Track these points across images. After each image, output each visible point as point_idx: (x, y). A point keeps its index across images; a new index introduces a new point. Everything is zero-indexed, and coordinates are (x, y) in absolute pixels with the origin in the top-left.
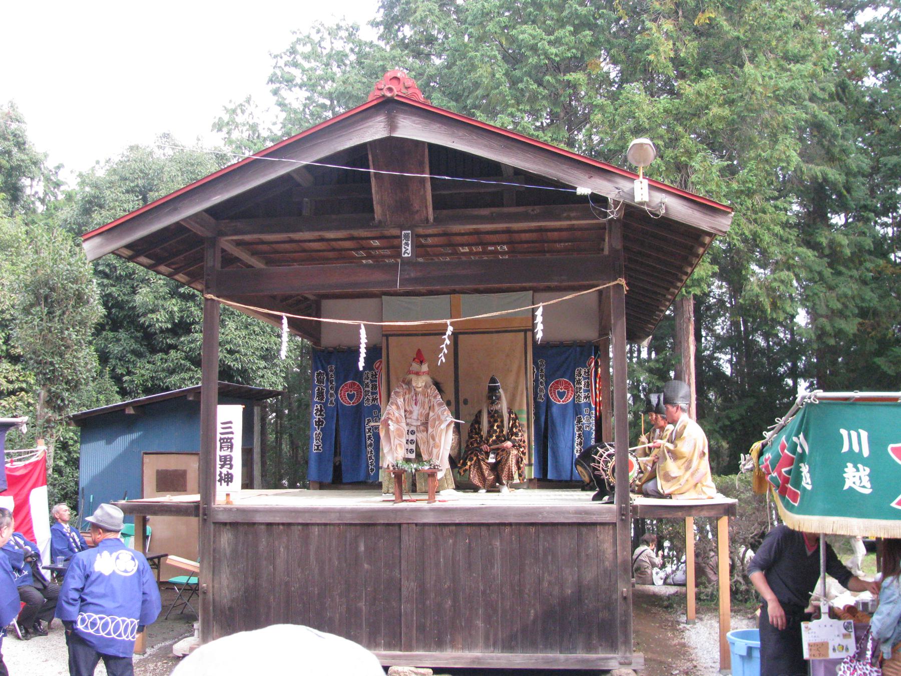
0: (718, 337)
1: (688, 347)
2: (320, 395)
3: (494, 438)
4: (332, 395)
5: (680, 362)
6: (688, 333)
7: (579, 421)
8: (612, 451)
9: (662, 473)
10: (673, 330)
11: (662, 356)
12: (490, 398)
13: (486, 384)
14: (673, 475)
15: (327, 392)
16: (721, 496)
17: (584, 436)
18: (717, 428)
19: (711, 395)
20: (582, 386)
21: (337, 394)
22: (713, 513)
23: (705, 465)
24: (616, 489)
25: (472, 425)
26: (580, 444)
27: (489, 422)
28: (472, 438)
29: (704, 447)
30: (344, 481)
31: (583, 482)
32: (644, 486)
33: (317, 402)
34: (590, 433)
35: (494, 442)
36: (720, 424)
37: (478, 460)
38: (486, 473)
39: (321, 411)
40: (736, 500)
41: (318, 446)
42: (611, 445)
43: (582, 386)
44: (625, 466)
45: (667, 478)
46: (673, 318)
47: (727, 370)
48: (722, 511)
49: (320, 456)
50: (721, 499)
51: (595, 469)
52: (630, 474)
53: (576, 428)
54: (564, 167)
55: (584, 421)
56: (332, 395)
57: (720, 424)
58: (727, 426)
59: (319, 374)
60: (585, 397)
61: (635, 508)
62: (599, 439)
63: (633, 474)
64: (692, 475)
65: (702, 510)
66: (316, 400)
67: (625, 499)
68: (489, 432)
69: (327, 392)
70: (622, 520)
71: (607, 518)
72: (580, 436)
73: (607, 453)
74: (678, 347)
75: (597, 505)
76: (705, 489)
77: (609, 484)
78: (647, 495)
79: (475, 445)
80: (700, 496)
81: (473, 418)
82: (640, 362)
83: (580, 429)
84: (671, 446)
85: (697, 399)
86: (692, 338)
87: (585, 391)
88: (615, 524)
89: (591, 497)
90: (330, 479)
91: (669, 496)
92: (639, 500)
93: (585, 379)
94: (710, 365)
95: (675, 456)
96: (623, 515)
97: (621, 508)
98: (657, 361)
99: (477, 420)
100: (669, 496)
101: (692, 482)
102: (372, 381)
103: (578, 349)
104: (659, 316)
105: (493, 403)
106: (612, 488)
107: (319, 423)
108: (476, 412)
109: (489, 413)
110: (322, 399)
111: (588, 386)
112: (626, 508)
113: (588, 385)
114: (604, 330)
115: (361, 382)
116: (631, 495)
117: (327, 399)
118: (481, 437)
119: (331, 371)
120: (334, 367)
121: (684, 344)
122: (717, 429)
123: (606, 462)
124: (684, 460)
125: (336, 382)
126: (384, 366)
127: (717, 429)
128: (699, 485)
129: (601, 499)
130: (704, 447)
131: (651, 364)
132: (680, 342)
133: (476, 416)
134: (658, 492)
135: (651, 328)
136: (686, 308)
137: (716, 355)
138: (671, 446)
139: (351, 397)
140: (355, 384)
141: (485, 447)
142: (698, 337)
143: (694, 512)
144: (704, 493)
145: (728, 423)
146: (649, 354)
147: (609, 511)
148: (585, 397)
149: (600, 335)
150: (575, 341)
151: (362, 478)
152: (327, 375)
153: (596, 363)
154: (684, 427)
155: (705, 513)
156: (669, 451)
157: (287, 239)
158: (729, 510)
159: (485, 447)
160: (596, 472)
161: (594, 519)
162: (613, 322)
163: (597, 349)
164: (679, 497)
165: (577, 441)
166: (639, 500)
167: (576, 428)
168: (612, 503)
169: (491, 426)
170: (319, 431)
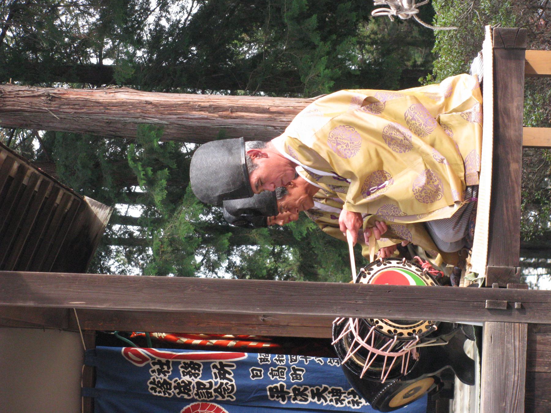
0: (103, 29)
1: (122, 104)
5: (159, 128)
6: (86, 103)
7: (281, 393)
8: (352, 325)
9: (418, 207)
10: (78, 137)
11: (139, 171)
14: (423, 180)
16: (476, 64)
17: (317, 385)
18: (324, 47)
19: (249, 51)
20: (194, 381)
22: (516, 87)
23: (398, 101)
24: (447, 319)
26: (336, 393)
29: (354, 101)
31: (431, 393)
32: (445, 249)
34: (311, 369)
36: (316, 39)
40: (487, 28)
42: (339, 329)
43: (194, 381)
44: (394, 296)
45: (429, 194)
46: (51, 135)
48: (513, 65)
50: (483, 65)
51: (395, 373)
52: (412, 283)
53: (298, 402)
55: (281, 382)
57: (316, 39)
58: (321, 20)
60: (223, 374)
61: (493, 275)
62: (322, 347)
63: (412, 276)
64: (419, 133)
65: (507, 113)
67: (472, 300)
70: (522, 309)
71: (517, 345)
72: (318, 395)
73: (357, 338)
74: (122, 128)
75: (484, 373)
76: (455, 103)
77: (433, 334)
78: (466, 244)
80: (475, 116)
82: (148, 222)
83: (299, 393)
84: (354, 188)
85: (253, 91)
86: (101, 95)
87: (207, 374)
88: (532, 328)
89: (467, 387)
91: (469, 192)
92: (478, 262)
93: (176, 373)
94: (176, 51)
95: (375, 177)
96: (510, 307)
97: (494, 311)
98: (151, 183)
100: (469, 192)
101: (436, 132)
103: (100, 386)
104: (34, 178)
106: (444, 328)
111: (196, 367)
112: (494, 297)
113: (192, 366)
114: (61, 319)
116: (464, 284)
121: (114, 114)
122: (327, 47)
123: (380, 340)
124: (384, 155)
127: (327, 47)
128: (444, 117)
129: (471, 363)
130: (354, 101)
131: (158, 197)
132: (109, 123)
134: (459, 217)
135: (66, 199)
136: (24, 104)
137: (146, 36)
138: (354, 188)
142: (101, 77)
143: (511, 133)
144: (465, 105)
145: (313, 20)
146: (133, 199)
147: (499, 340)
148: (223, 374)
149: (71, 327)
150: (82, 392)
153: (142, 342)
154: (303, 148)
155: (517, 105)
156: (364, 191)
158: (510, 49)
160: (404, 370)
161: (517, 377)
162: (31, 304)
163: (104, 338)
164: (472, 170)
165: (328, 402)
166: (478, 262)
167: (298, 402)
168: (479, 331)
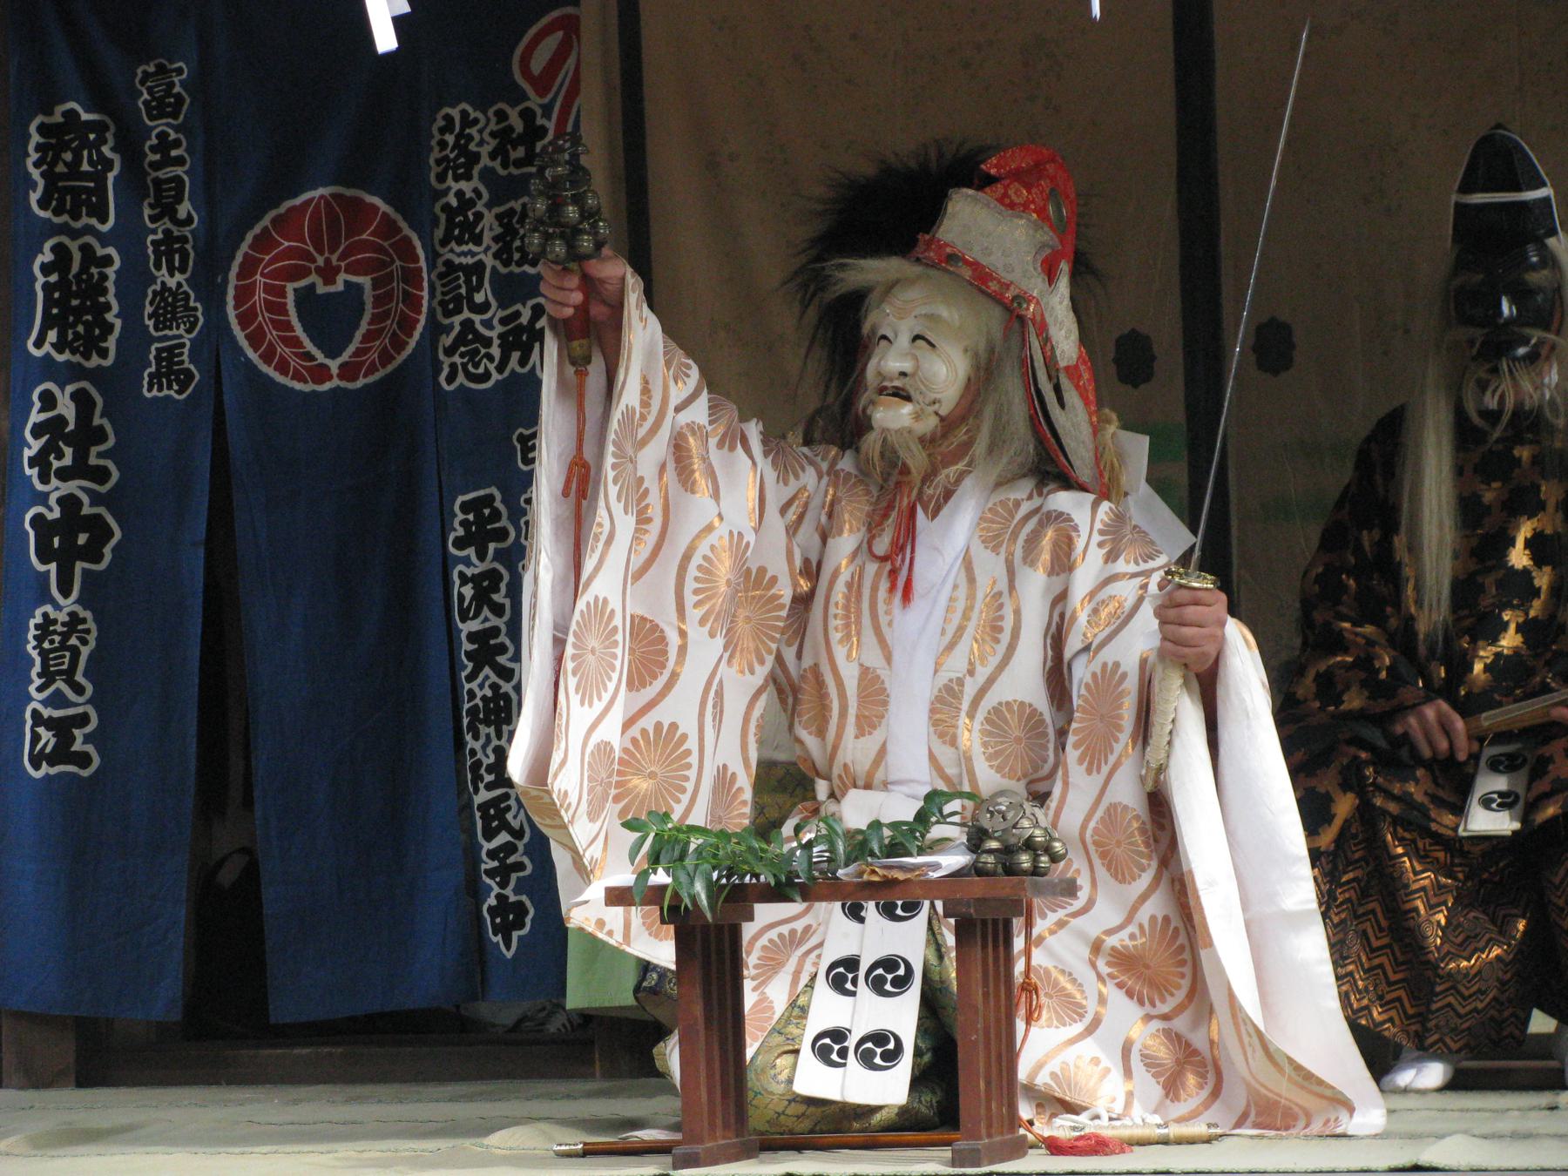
2: (76, 305)
3: (1510, 641)
4: (170, 308)
12: (1468, 305)
13: (1438, 195)
15: (135, 279)
21: (213, 296)
25: (1333, 539)
27: (1469, 510)
28: (1337, 644)
30: (283, 1010)
33: (47, 368)
35: (1513, 676)
37: (1366, 814)
38: (1434, 922)
39: (86, 436)
41: (62, 728)
47: (1555, 371)
49: (75, 804)
54: (560, 561)
56: (170, 308)
59: (58, 137)
66: (40, 346)
68: (1464, 591)
69: (135, 279)
79: (1354, 701)
81: (1338, 477)
90: (163, 996)
99: (1370, 501)
102: (502, 189)
105: (1496, 346)
107: (69, 536)
108: (1359, 428)
109: (1465, 434)
110: (92, 345)
115: (411, 195)
117: (135, 338)
118: (1404, 639)
119: (159, 109)
120: (182, 72)
125: (209, 202)
126: (594, 56)
133: (1363, 461)
139: (329, 319)
140: (358, 213)
141: (1432, 722)
151: (426, 979)
152: (130, 147)
157: (567, 509)
159: (1432, 722)
169: (1483, 544)
170: (66, 606)
